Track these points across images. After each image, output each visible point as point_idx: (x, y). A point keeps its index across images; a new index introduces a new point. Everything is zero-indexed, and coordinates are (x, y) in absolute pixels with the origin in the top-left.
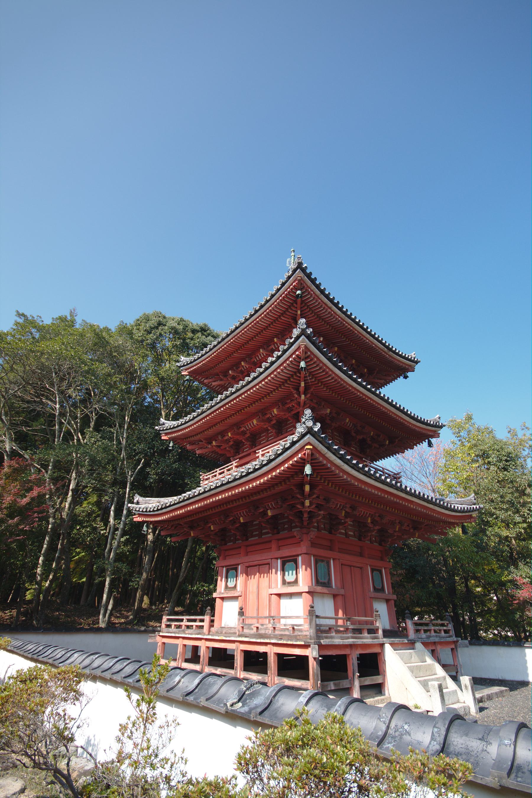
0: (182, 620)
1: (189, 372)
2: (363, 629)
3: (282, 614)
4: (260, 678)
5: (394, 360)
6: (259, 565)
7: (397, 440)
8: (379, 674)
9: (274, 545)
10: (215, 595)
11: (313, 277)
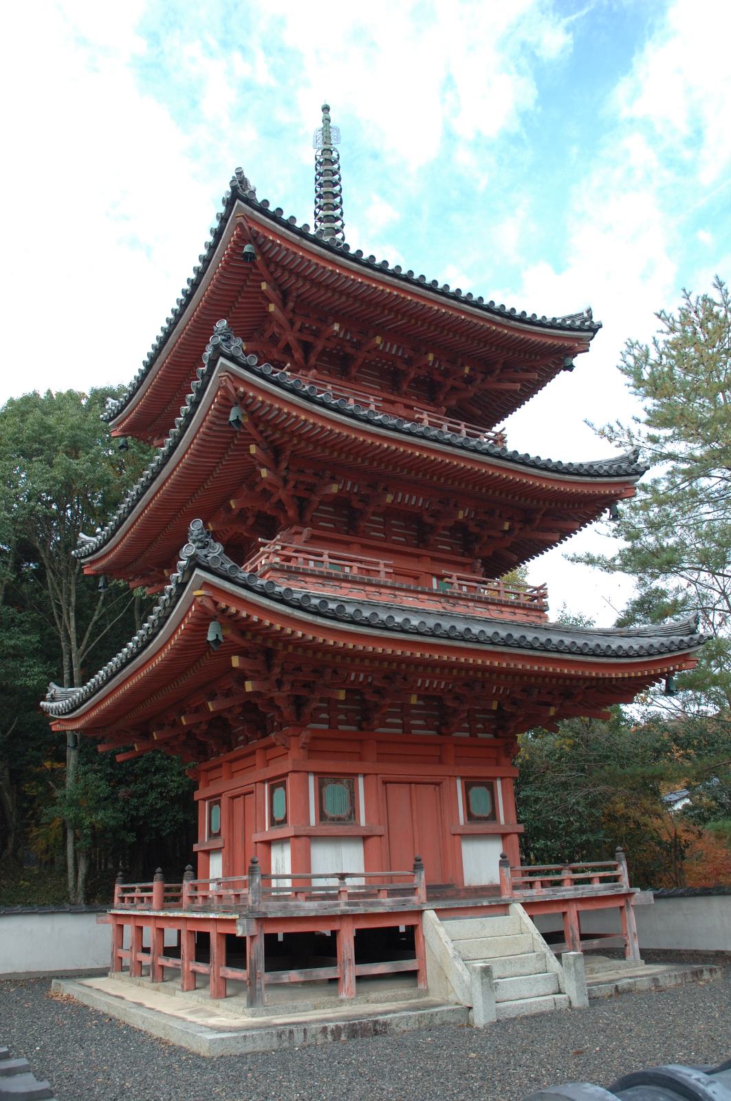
0: (133, 890)
1: (121, 430)
2: (563, 880)
3: (315, 871)
4: (207, 969)
5: (528, 337)
6: (245, 794)
7: (539, 517)
8: (414, 957)
9: (258, 759)
10: (196, 848)
11: (272, 208)
